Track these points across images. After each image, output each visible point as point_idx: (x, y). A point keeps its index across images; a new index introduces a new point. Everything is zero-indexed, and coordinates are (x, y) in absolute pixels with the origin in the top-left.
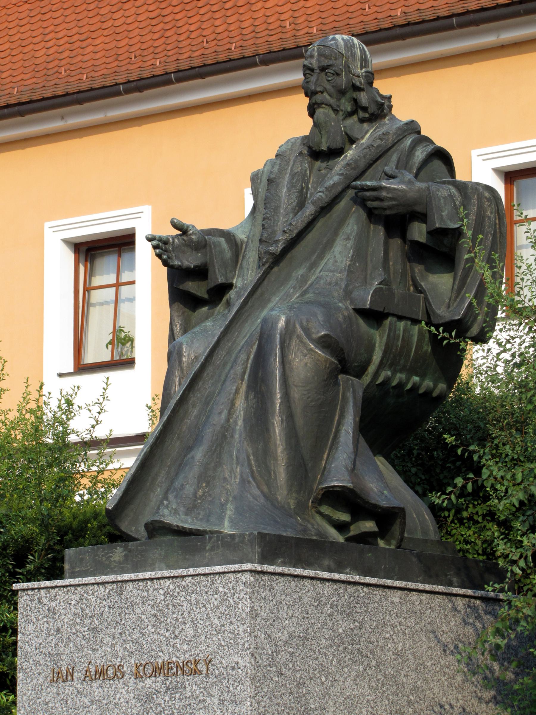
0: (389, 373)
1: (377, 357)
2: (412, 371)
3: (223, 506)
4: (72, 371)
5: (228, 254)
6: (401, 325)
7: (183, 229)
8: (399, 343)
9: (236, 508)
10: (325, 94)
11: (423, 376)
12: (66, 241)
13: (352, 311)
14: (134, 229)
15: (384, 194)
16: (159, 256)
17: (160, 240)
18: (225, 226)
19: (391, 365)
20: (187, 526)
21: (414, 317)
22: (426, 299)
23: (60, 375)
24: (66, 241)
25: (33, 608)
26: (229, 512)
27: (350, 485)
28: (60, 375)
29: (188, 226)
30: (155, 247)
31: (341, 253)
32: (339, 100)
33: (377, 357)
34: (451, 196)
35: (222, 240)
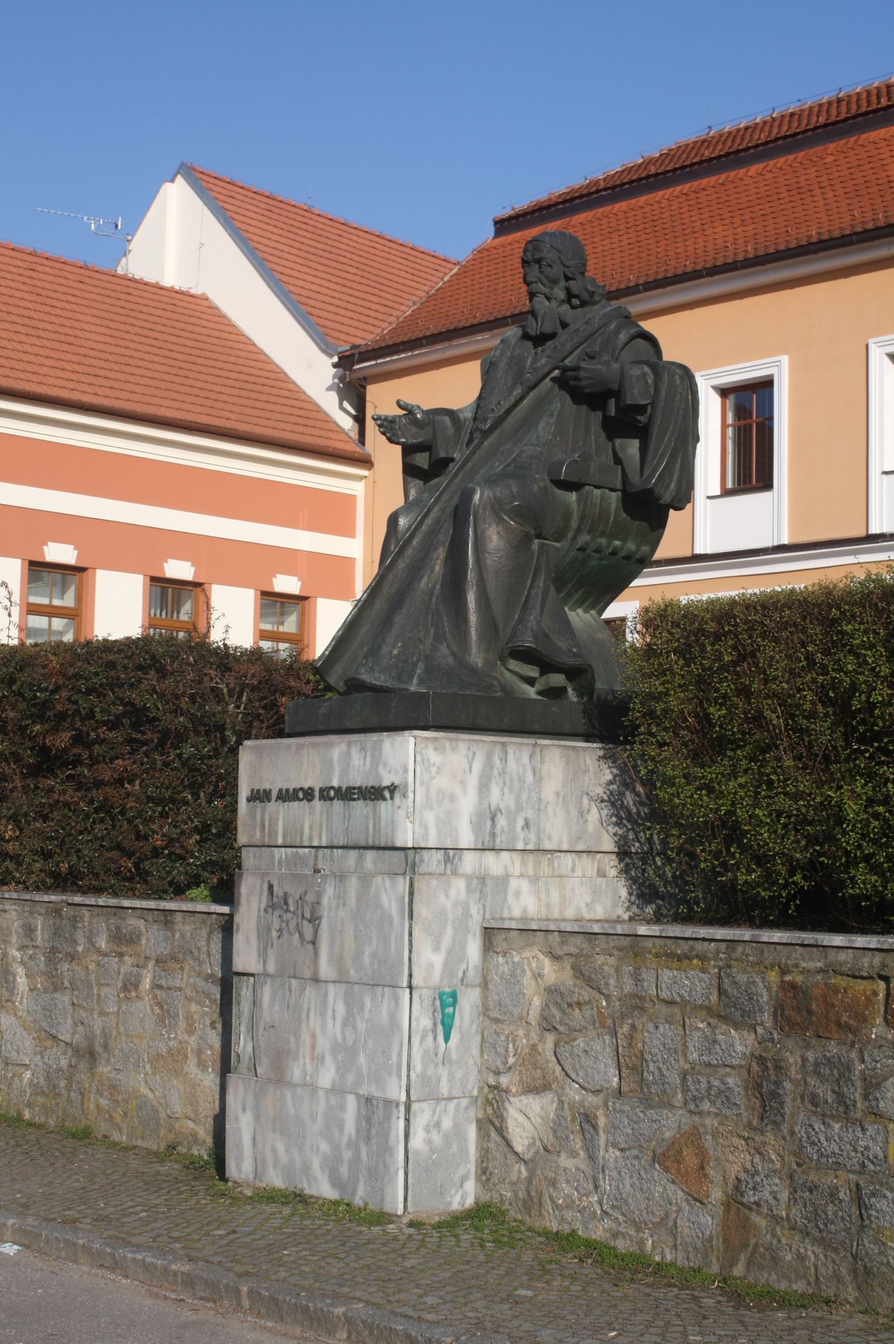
0: (588, 538)
1: (574, 524)
2: (613, 536)
3: (415, 665)
4: (718, 493)
5: (451, 432)
6: (597, 492)
7: (409, 410)
8: (597, 511)
9: (425, 667)
10: (539, 284)
11: (624, 540)
12: (715, 388)
13: (548, 482)
14: (772, 376)
15: (582, 374)
16: (383, 433)
17: (386, 419)
18: (454, 407)
19: (589, 531)
20: (378, 683)
21: (612, 486)
22: (623, 470)
23: (709, 498)
24: (715, 388)
25: (210, 762)
26: (418, 671)
27: (534, 646)
28: (709, 498)
29: (413, 406)
30: (380, 426)
31: (544, 429)
32: (552, 289)
33: (574, 524)
34: (644, 375)
35: (447, 419)
